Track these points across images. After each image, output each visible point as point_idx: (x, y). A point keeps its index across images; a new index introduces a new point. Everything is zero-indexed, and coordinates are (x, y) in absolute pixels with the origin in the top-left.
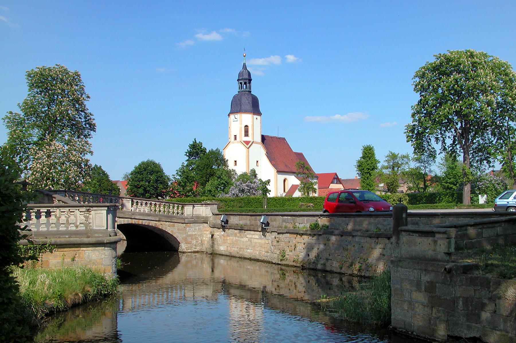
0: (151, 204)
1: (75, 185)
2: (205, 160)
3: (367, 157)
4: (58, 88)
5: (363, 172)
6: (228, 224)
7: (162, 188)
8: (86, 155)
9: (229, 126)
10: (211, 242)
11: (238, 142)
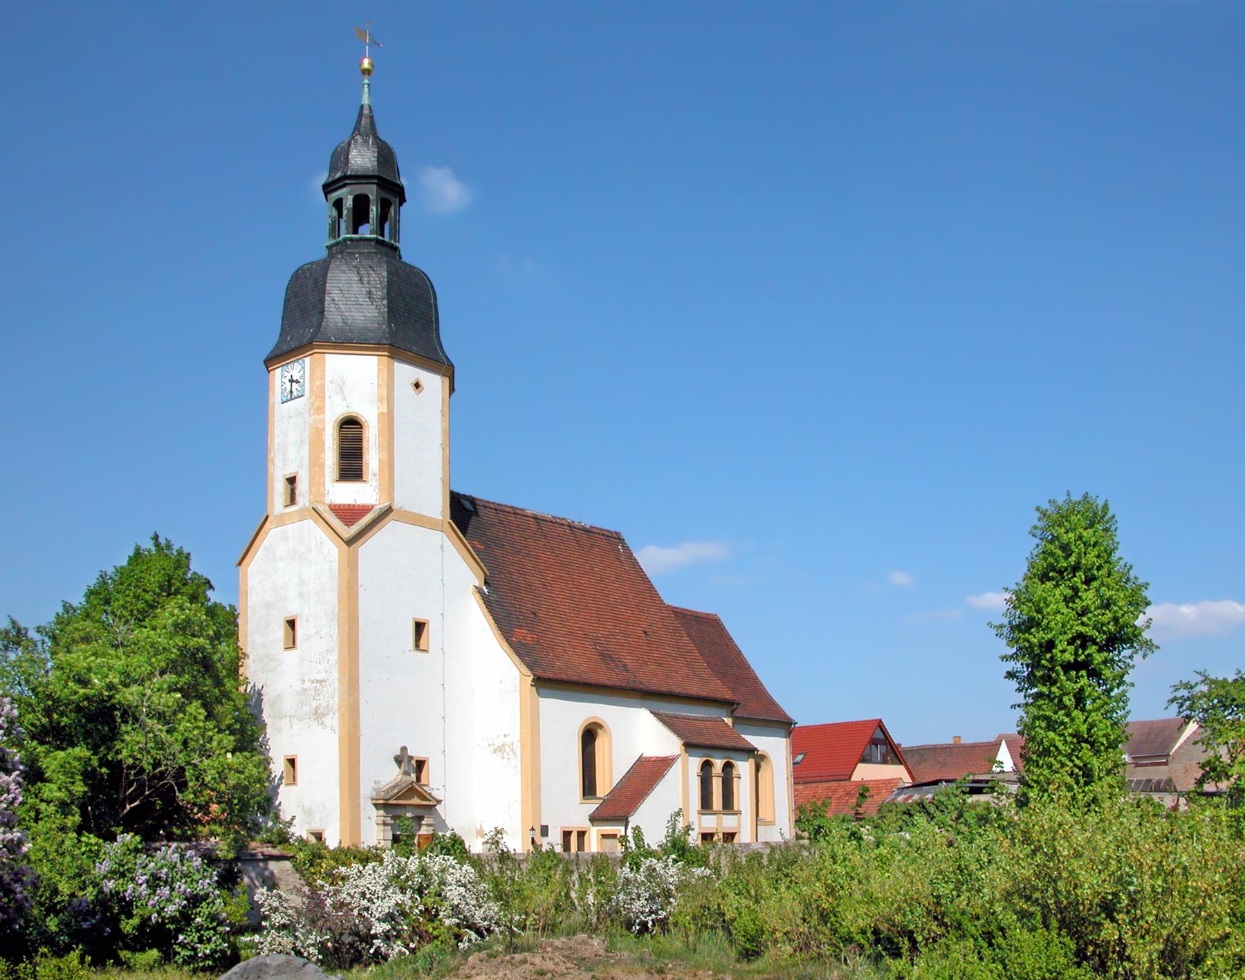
11: (302, 516)
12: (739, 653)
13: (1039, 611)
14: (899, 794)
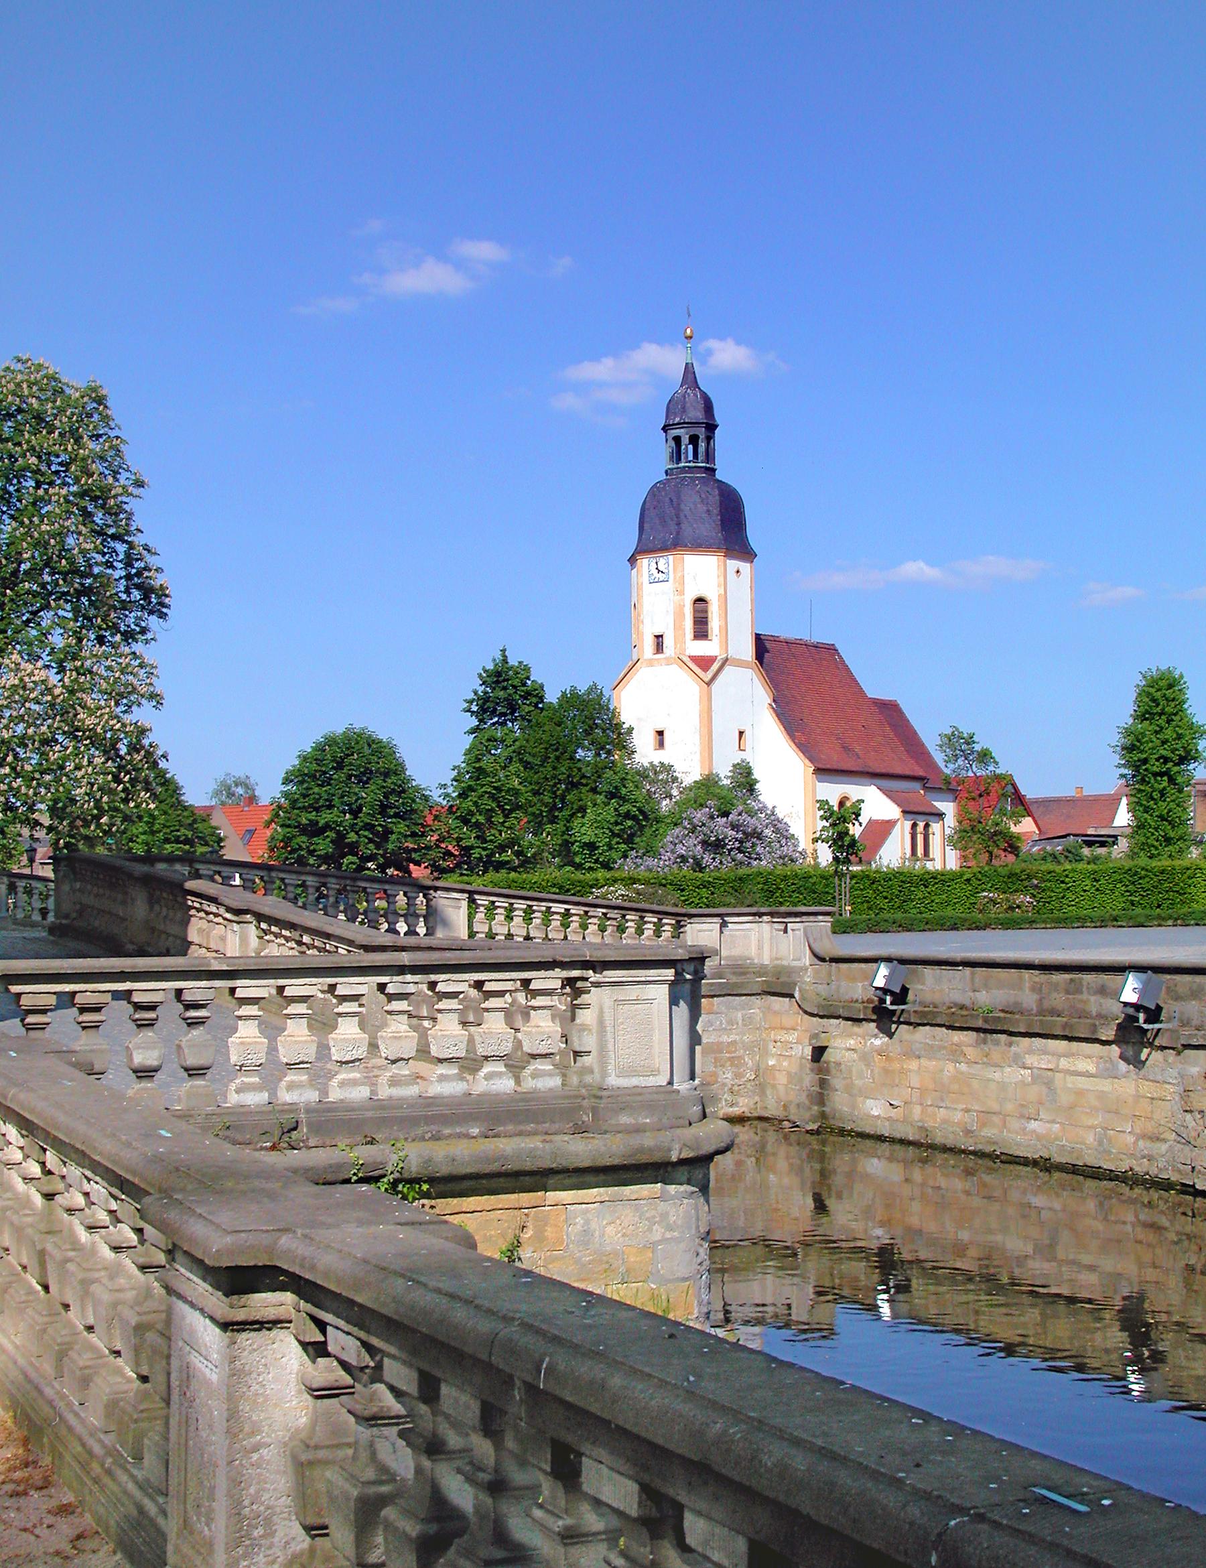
1: (99, 826)
2: (546, 728)
3: (1160, 714)
4: (25, 447)
5: (1146, 770)
6: (904, 1003)
7: (406, 836)
8: (134, 708)
9: (634, 599)
10: (809, 1079)
11: (668, 662)
12: (915, 733)
13: (1139, 741)
14: (1033, 846)
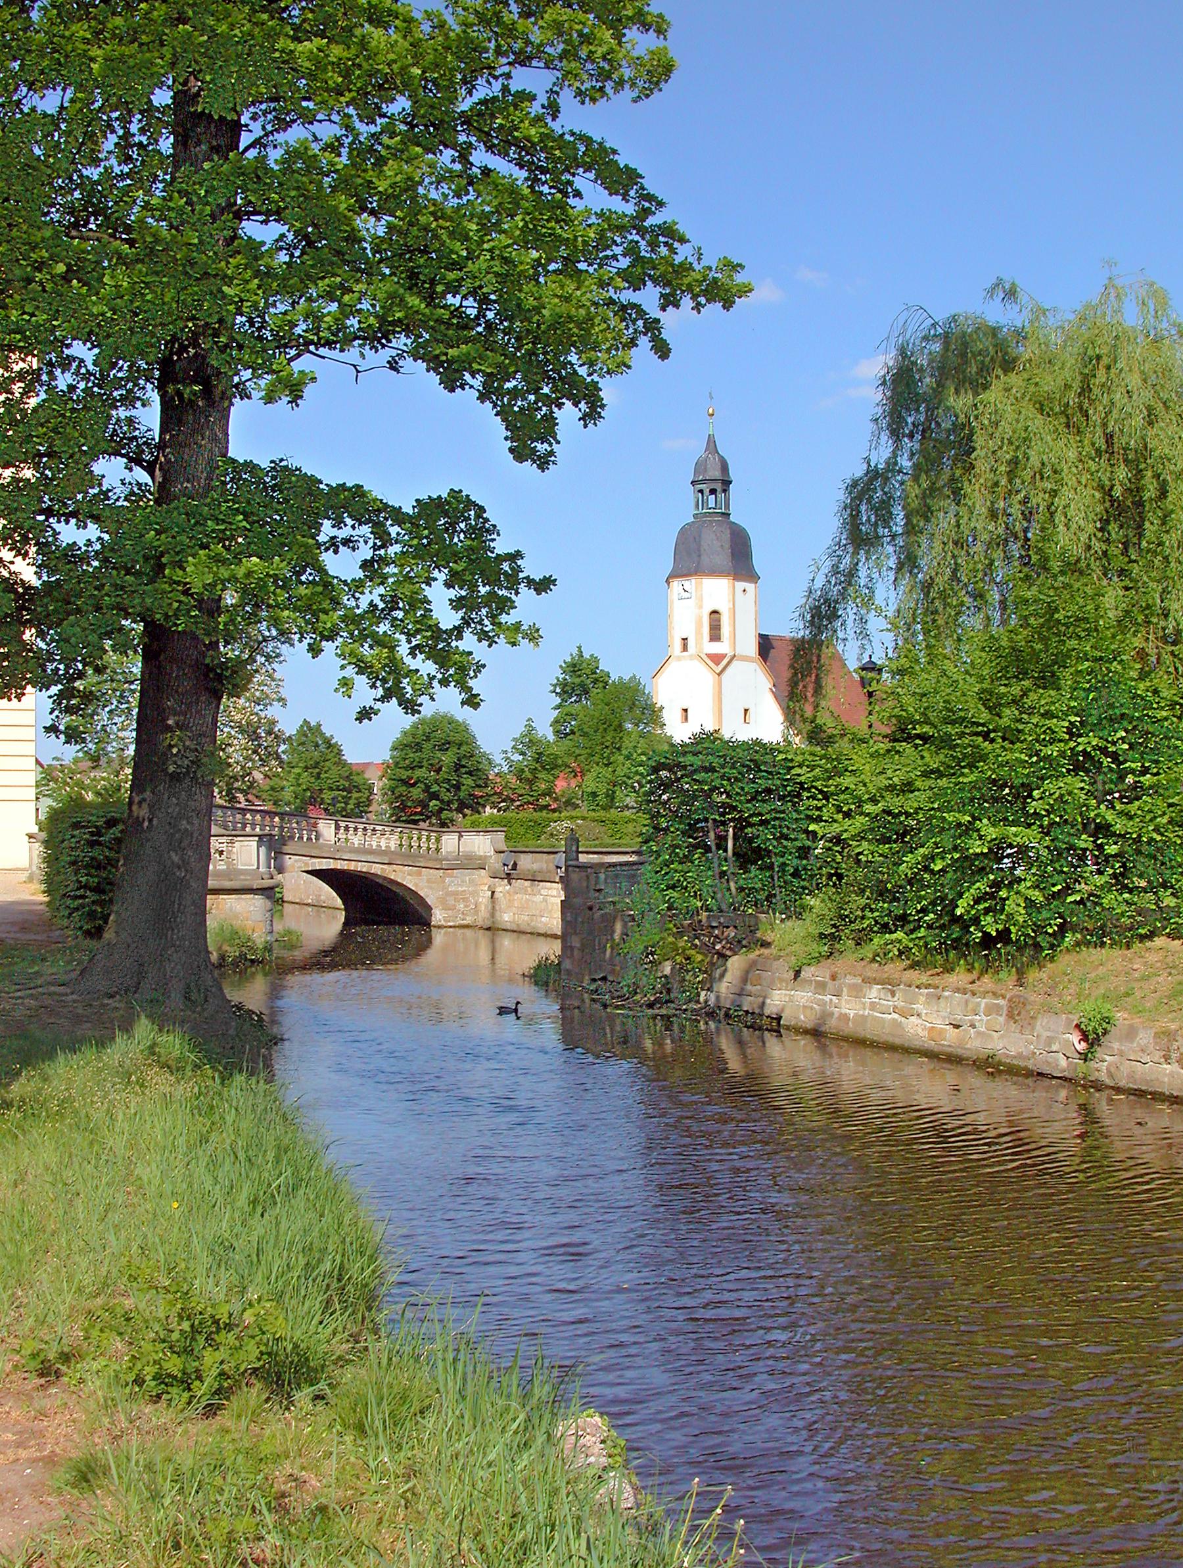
0: (365, 829)
1: (244, 782)
11: (691, 658)
